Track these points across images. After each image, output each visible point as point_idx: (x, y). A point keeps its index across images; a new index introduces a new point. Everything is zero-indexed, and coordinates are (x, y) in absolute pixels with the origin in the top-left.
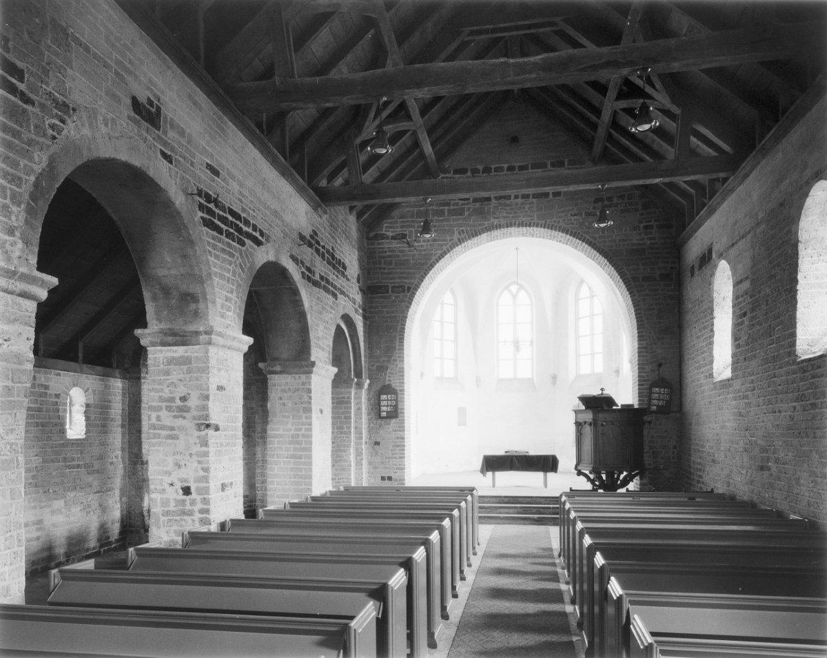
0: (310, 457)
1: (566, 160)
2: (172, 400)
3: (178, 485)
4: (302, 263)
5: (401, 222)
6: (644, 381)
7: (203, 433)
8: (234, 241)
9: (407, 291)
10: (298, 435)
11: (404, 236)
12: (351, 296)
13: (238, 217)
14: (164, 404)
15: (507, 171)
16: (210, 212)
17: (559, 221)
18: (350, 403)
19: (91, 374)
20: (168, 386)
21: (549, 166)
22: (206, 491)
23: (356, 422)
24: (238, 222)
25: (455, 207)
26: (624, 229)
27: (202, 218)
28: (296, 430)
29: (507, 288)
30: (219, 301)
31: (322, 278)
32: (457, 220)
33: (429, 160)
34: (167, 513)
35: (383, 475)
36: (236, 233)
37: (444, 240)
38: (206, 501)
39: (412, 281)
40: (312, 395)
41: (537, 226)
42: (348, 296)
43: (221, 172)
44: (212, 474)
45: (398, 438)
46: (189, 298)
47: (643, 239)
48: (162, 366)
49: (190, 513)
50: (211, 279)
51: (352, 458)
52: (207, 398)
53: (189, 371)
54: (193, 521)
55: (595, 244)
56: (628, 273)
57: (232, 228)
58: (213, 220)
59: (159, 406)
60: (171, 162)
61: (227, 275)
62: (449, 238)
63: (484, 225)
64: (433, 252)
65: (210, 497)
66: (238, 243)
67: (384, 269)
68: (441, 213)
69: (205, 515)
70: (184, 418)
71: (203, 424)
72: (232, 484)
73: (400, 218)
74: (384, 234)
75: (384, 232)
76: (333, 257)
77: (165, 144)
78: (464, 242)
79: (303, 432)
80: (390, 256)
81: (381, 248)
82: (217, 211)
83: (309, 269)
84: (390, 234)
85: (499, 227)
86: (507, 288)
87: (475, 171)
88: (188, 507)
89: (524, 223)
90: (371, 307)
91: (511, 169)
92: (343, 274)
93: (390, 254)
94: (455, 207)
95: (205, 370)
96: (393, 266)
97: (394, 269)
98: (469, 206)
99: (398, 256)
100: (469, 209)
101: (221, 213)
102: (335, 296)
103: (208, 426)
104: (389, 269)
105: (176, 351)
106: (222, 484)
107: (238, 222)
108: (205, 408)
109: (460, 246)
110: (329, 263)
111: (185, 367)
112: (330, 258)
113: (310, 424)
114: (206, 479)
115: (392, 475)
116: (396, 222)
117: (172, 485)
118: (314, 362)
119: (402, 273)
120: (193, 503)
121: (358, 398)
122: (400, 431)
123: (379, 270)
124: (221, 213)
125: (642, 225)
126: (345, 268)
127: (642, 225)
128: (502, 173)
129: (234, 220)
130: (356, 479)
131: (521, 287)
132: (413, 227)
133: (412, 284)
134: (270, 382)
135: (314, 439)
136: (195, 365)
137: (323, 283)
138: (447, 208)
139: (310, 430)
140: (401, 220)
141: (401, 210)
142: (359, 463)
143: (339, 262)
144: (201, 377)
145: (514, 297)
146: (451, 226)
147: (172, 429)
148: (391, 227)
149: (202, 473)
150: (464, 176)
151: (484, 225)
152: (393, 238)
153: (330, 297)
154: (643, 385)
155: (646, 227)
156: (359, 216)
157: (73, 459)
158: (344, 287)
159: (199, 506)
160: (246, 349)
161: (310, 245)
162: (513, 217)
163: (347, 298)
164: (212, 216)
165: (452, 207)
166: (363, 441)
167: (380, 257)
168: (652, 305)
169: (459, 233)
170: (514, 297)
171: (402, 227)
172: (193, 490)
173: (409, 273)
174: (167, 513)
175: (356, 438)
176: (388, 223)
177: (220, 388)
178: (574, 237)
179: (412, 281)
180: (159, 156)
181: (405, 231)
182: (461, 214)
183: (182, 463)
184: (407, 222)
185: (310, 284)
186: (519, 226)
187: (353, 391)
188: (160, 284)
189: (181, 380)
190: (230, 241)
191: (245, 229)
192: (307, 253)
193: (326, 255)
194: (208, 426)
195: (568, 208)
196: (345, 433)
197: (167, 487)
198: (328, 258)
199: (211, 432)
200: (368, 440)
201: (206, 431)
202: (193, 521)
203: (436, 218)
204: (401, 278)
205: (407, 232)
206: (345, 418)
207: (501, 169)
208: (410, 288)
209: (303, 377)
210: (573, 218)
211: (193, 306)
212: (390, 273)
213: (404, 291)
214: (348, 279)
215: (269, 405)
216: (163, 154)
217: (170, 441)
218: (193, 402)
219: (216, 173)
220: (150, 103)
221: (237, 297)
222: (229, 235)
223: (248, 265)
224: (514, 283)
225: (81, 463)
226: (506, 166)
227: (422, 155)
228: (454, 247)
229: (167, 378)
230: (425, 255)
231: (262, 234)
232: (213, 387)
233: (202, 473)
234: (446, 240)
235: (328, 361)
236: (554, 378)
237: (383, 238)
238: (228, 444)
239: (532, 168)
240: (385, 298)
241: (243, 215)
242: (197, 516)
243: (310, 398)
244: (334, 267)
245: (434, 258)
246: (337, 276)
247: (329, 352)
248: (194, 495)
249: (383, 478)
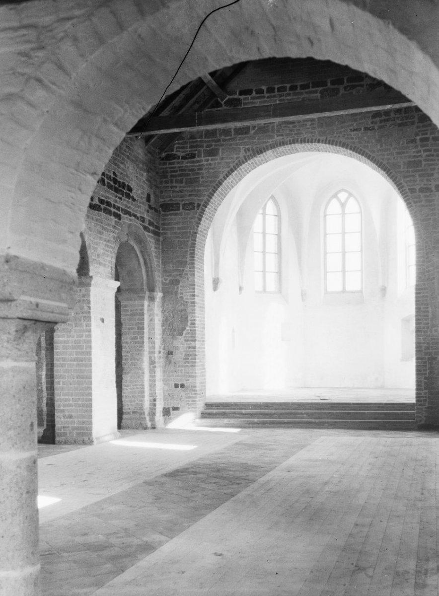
0: (90, 360)
1: (345, 78)
5: (191, 142)
6: (422, 289)
10: (80, 340)
11: (193, 156)
15: (290, 90)
17: (339, 137)
18: (143, 314)
21: (329, 84)
23: (150, 333)
26: (401, 143)
28: (78, 336)
29: (335, 196)
31: (102, 201)
32: (243, 139)
35: (177, 383)
37: (231, 158)
40: (92, 305)
41: (319, 142)
42: (135, 216)
45: (190, 348)
47: (420, 151)
51: (146, 365)
55: (374, 157)
56: (405, 184)
63: (268, 142)
67: (176, 187)
73: (190, 139)
74: (175, 155)
75: (175, 153)
76: (115, 181)
78: (249, 159)
79: (84, 338)
80: (181, 175)
81: (172, 168)
84: (181, 154)
85: (283, 144)
86: (335, 196)
87: (260, 91)
89: (241, 161)
90: (164, 224)
91: (292, 88)
92: (128, 196)
99: (188, 175)
102: (118, 217)
104: (180, 187)
110: (110, 187)
112: (112, 183)
113: (90, 331)
115: (184, 382)
116: (186, 143)
118: (92, 276)
119: (192, 191)
121: (150, 310)
123: (170, 189)
125: (418, 138)
126: (130, 189)
127: (418, 138)
128: (285, 93)
131: (350, 195)
132: (202, 146)
133: (202, 200)
135: (93, 345)
137: (102, 206)
139: (90, 336)
142: (152, 371)
143: (123, 185)
145: (343, 205)
150: (249, 97)
151: (268, 142)
152: (184, 158)
153: (112, 218)
154: (420, 293)
155: (422, 140)
158: (129, 207)
162: (295, 134)
163: (133, 218)
167: (171, 176)
168: (428, 215)
169: (245, 151)
170: (343, 205)
175: (150, 348)
176: (178, 144)
178: (353, 151)
182: (246, 133)
186: (301, 142)
187: (146, 303)
193: (106, 180)
195: (348, 124)
196: (139, 343)
198: (108, 183)
200: (161, 350)
203: (223, 137)
204: (191, 195)
207: (284, 89)
209: (83, 290)
210: (352, 133)
212: (181, 191)
213: (194, 208)
214: (134, 200)
224: (343, 190)
226: (288, 86)
235: (110, 275)
236: (384, 290)
237: (174, 158)
239: (313, 87)
240: (176, 215)
243: (89, 308)
244: (116, 190)
245: (221, 177)
246: (121, 199)
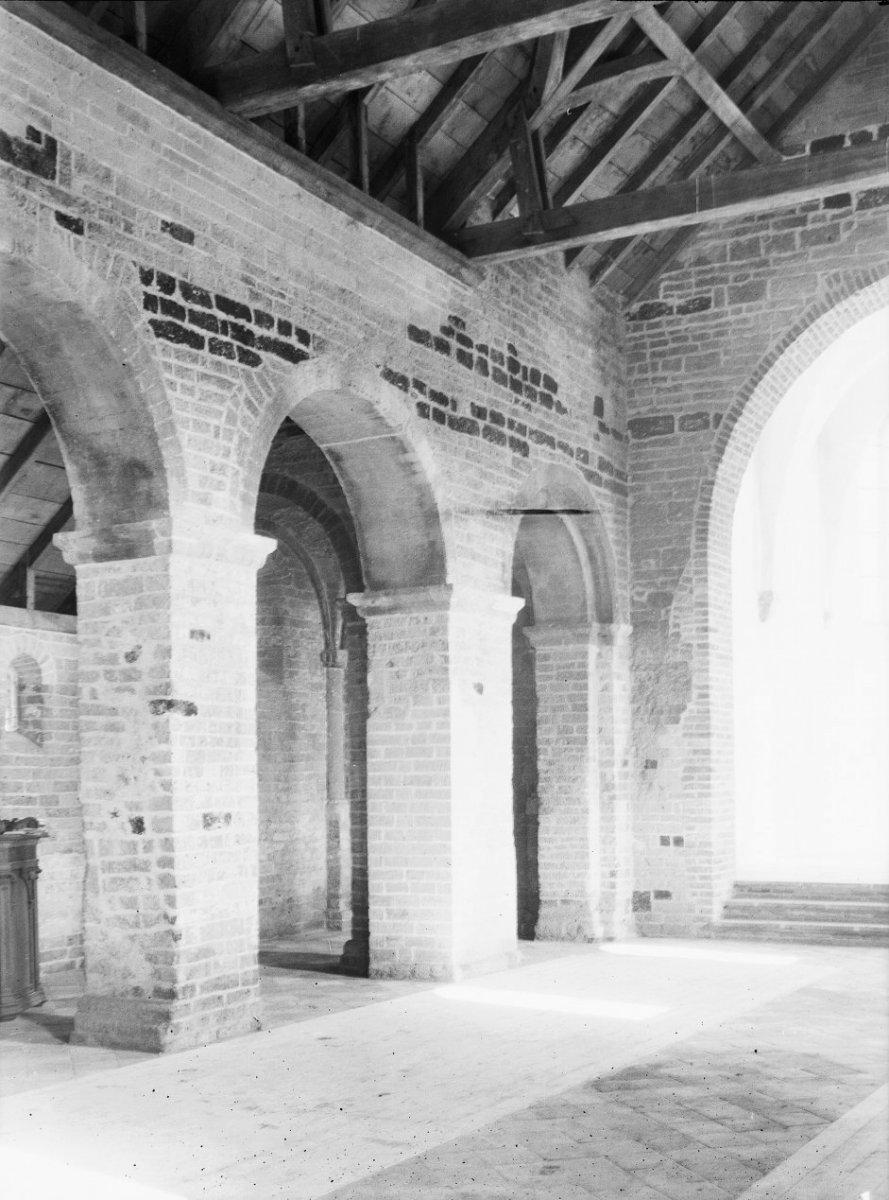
2: (113, 659)
3: (126, 815)
4: (420, 386)
7: (162, 718)
8: (230, 356)
9: (714, 425)
11: (704, 304)
12: (574, 445)
13: (243, 312)
14: (100, 668)
16: (171, 308)
19: (52, 630)
20: (107, 635)
22: (164, 826)
24: (241, 322)
25: (819, 225)
27: (152, 322)
30: (193, 473)
31: (480, 412)
33: (738, 133)
34: (109, 867)
36: (236, 343)
38: (168, 844)
39: (725, 401)
40: (452, 653)
42: (564, 447)
43: (196, 232)
44: (178, 794)
46: (137, 472)
48: (98, 599)
49: (144, 867)
50: (173, 431)
52: (167, 652)
53: (140, 604)
54: (149, 880)
57: (225, 333)
58: (179, 322)
59: (93, 672)
60: (79, 231)
61: (214, 422)
62: (804, 296)
64: (771, 331)
65: (173, 835)
66: (241, 361)
67: (664, 379)
68: (784, 243)
69: (166, 870)
70: (132, 691)
71: (161, 701)
72: (228, 817)
75: (661, 300)
76: (514, 366)
77: (68, 200)
80: (674, 351)
82: (188, 305)
83: (440, 398)
84: (675, 302)
88: (141, 856)
92: (547, 401)
93: (675, 345)
94: (819, 225)
95: (162, 601)
96: (683, 371)
97: (685, 378)
98: (849, 218)
100: (850, 225)
101: (198, 308)
102: (523, 449)
103: (170, 705)
104: (674, 379)
105: (119, 569)
106: (205, 816)
107: (241, 322)
108: (164, 671)
109: (832, 312)
111: (133, 598)
114: (167, 804)
115: (683, 834)
116: (687, 275)
117: (115, 814)
120: (148, 847)
121: (604, 664)
122: (702, 735)
124: (198, 308)
126: (552, 386)
129: (231, 318)
130: (878, 900)
132: (724, 280)
134: (371, 632)
136: (148, 593)
137: (481, 424)
138: (799, 229)
140: (698, 268)
141: (697, 247)
143: (535, 376)
144: (158, 615)
146: (809, 268)
147: (114, 711)
148: (678, 287)
149: (161, 792)
152: (683, 310)
156: (594, 273)
157: (19, 788)
159: (158, 853)
160: (260, 561)
161: (443, 347)
164: (175, 316)
165: (810, 227)
166: (618, 758)
169: (830, 283)
171: (698, 285)
172: (147, 824)
173: (718, 384)
174: (109, 867)
176: (670, 278)
177: (199, 634)
179: (725, 401)
180: (54, 223)
181: (709, 291)
183: (130, 775)
184: (712, 270)
185: (445, 428)
187: (593, 649)
188: (90, 449)
189: (126, 622)
190: (222, 359)
191: (259, 331)
192: (440, 370)
194: (170, 705)
196: (575, 741)
197: (107, 818)
199: (176, 717)
201: (167, 713)
202: (149, 880)
205: (712, 295)
206: (575, 708)
208: (721, 417)
211: (143, 486)
213: (706, 425)
215: (370, 679)
216: (63, 219)
217: (111, 735)
218: (145, 662)
219: (188, 237)
220: (34, 134)
221: (241, 463)
222: (216, 348)
223: (268, 400)
225: (34, 795)
227: (721, 129)
228: (818, 315)
229: (107, 618)
230: (753, 339)
231: (304, 337)
232: (179, 637)
233: (161, 792)
234: (800, 302)
235: (501, 584)
237: (660, 313)
238: (219, 742)
240: (666, 442)
241: (253, 306)
242: (156, 871)
243: (446, 659)
244: (516, 387)
245: (771, 346)
247: (504, 566)
248: (149, 833)
249: (664, 841)
